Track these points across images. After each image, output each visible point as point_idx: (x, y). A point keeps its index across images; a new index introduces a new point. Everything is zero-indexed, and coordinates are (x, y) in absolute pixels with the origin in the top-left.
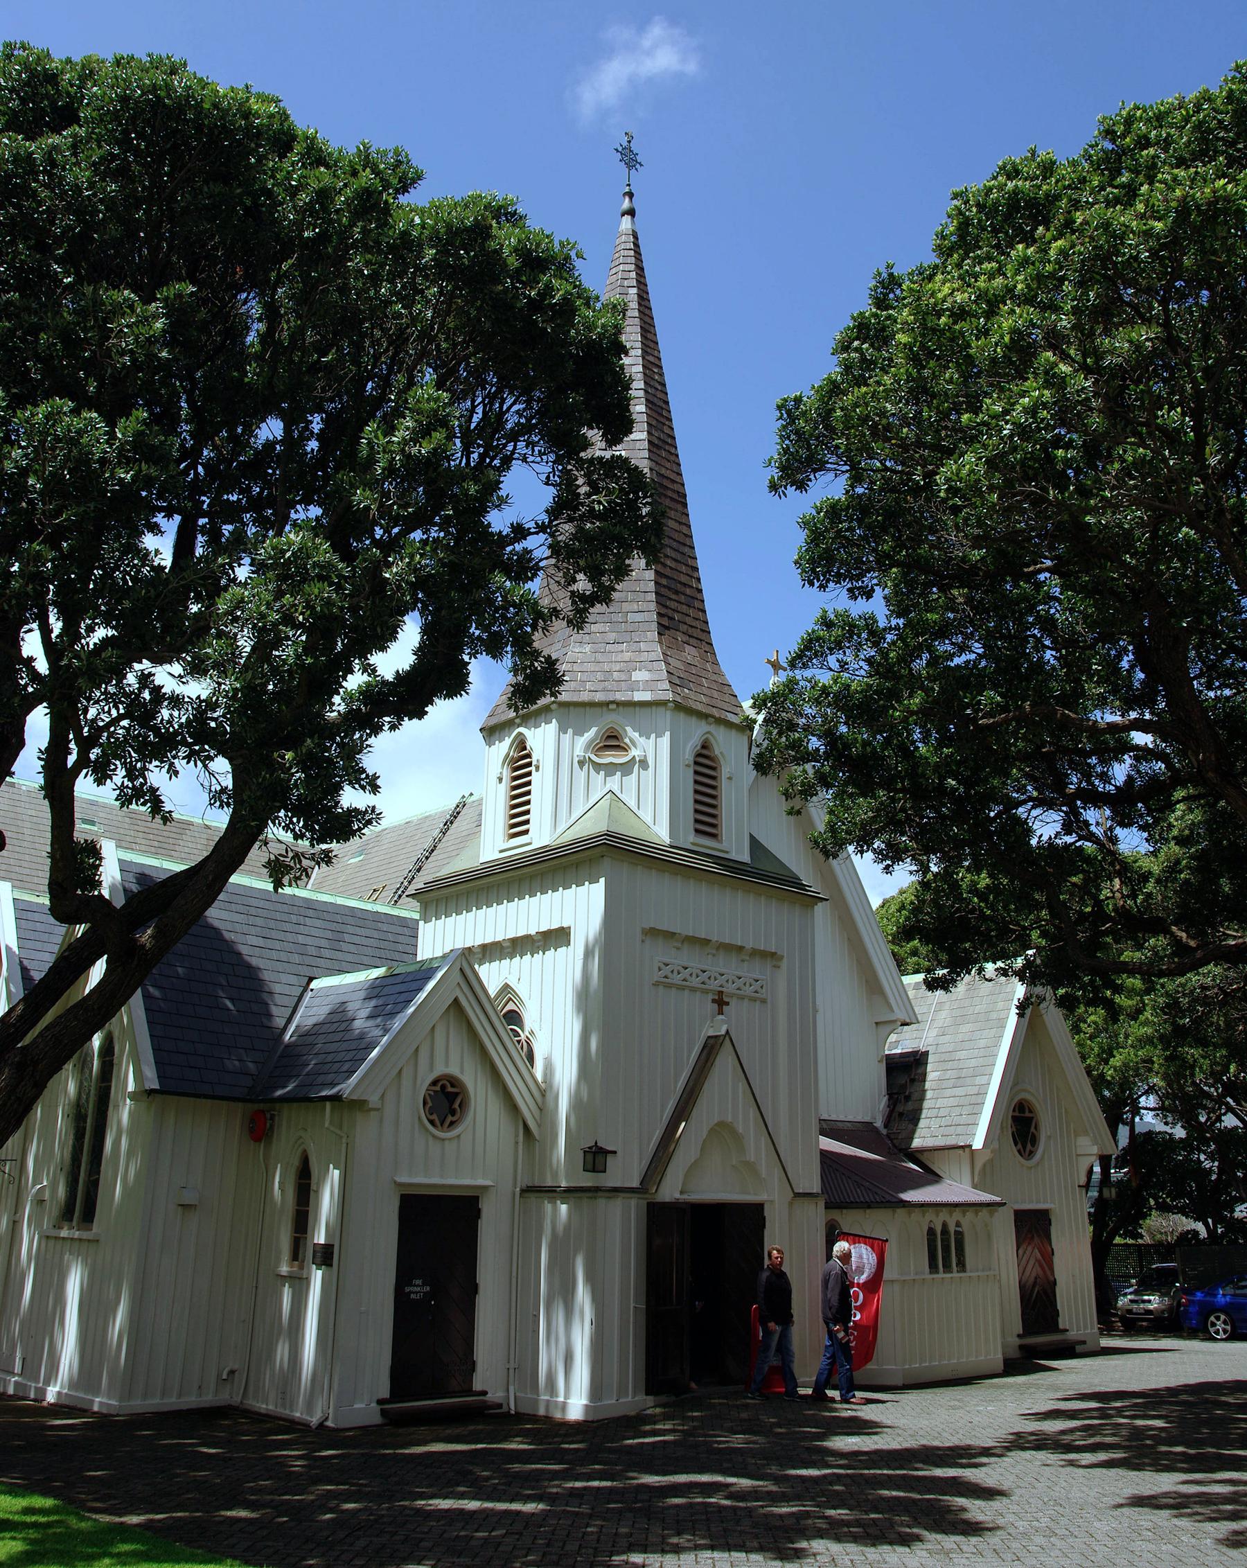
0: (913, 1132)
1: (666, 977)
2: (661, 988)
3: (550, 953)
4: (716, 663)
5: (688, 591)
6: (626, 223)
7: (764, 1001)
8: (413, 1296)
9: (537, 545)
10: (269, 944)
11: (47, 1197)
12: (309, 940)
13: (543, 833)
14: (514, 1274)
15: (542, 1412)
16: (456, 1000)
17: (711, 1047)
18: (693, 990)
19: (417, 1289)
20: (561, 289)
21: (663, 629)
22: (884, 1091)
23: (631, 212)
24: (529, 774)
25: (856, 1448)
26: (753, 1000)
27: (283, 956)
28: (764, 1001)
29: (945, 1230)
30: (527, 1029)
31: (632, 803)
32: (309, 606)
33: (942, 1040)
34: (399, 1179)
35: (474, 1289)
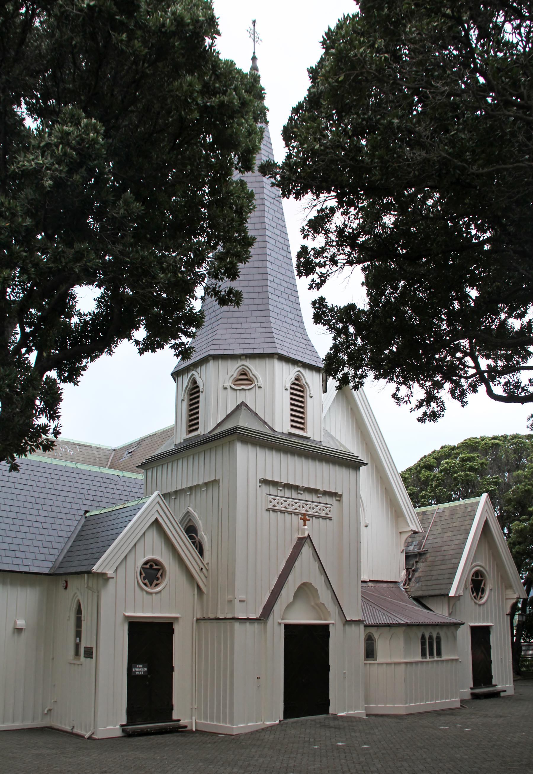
7: (330, 519)
16: (156, 520)
17: (301, 542)
18: (290, 513)
19: (140, 670)
26: (324, 518)
28: (330, 519)
33: (436, 541)
35: (490, 647)
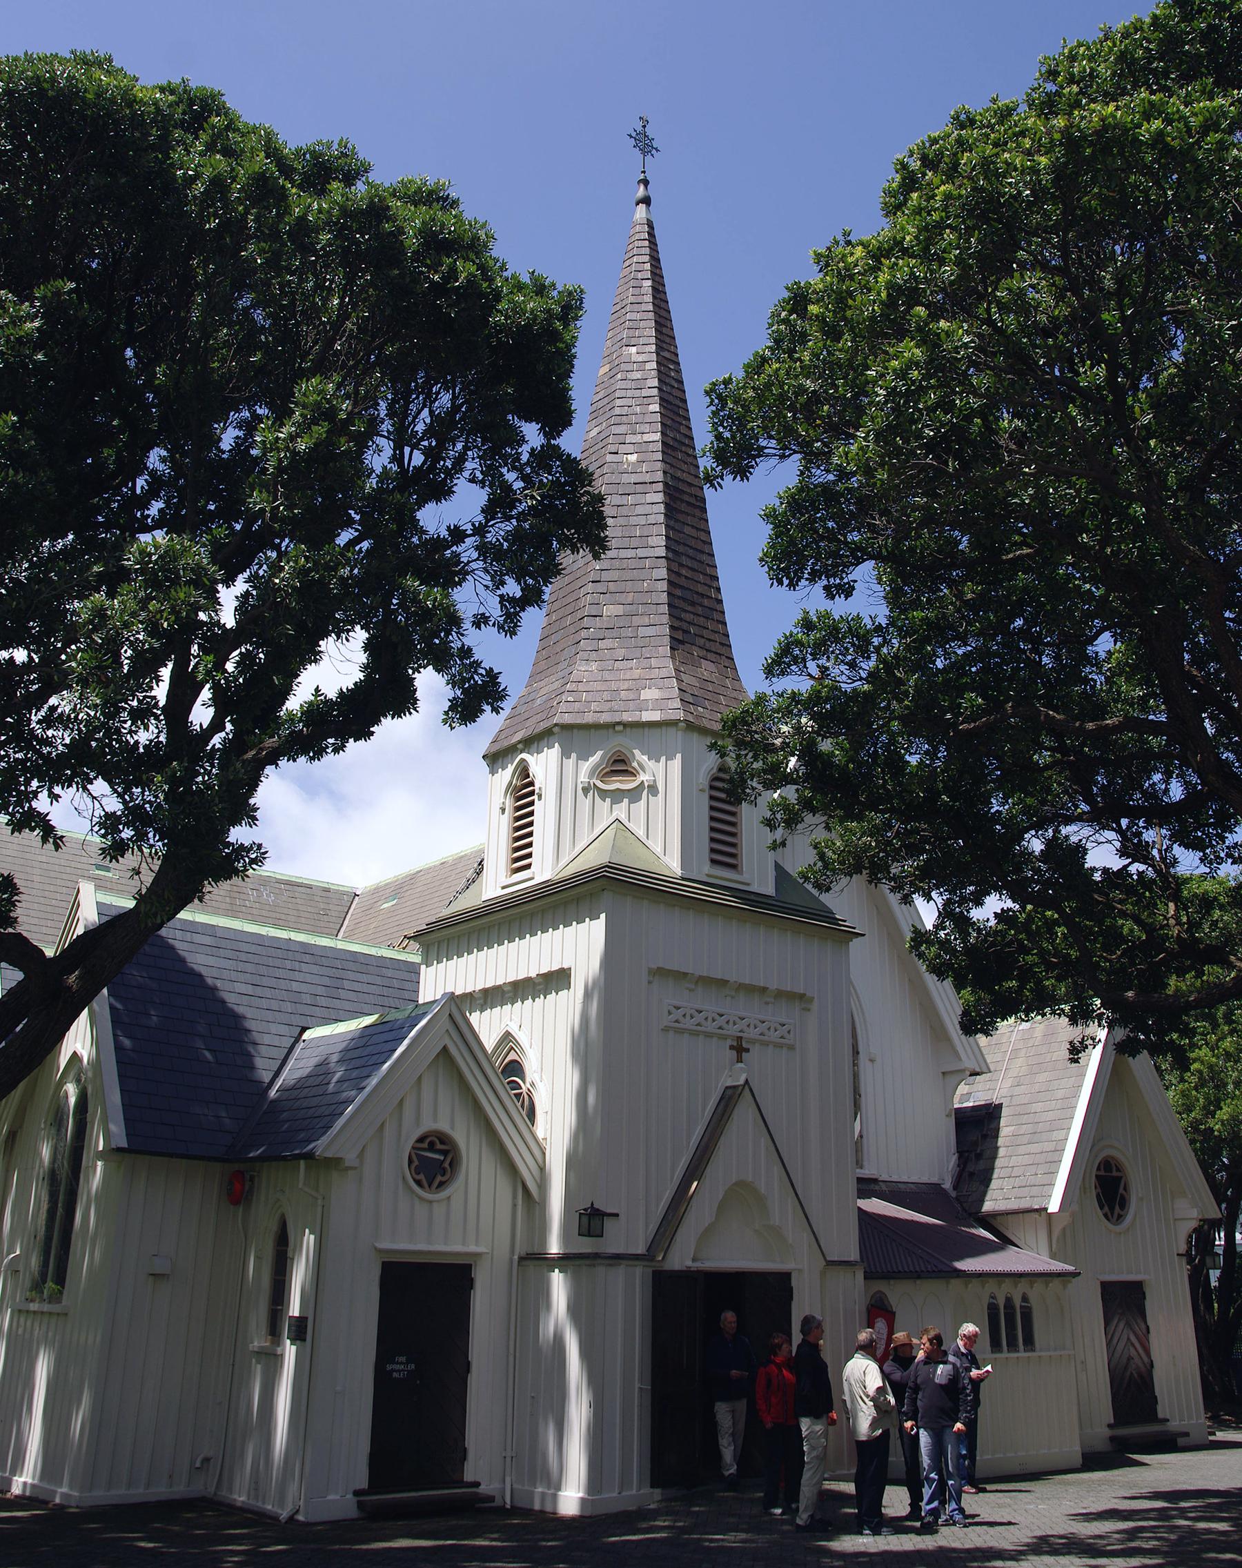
0: (984, 1194)
1: (677, 1021)
2: (671, 1033)
3: (552, 996)
4: (737, 679)
5: (706, 602)
6: (641, 212)
7: (791, 1048)
8: (395, 1375)
9: (467, 550)
10: (259, 991)
11: (21, 1268)
12: (303, 988)
13: (544, 869)
14: (512, 1351)
15: (537, 1507)
16: (445, 1048)
17: (729, 1098)
18: (708, 1035)
19: (400, 1367)
20: (466, 269)
21: (676, 643)
22: (953, 1148)
23: (646, 201)
24: (532, 803)
25: (863, 1549)
26: (778, 1046)
27: (274, 1005)
28: (791, 1048)
29: (1009, 1302)
30: (528, 1080)
31: (641, 833)
32: (174, 611)
33: (1018, 1090)
34: (377, 1245)
